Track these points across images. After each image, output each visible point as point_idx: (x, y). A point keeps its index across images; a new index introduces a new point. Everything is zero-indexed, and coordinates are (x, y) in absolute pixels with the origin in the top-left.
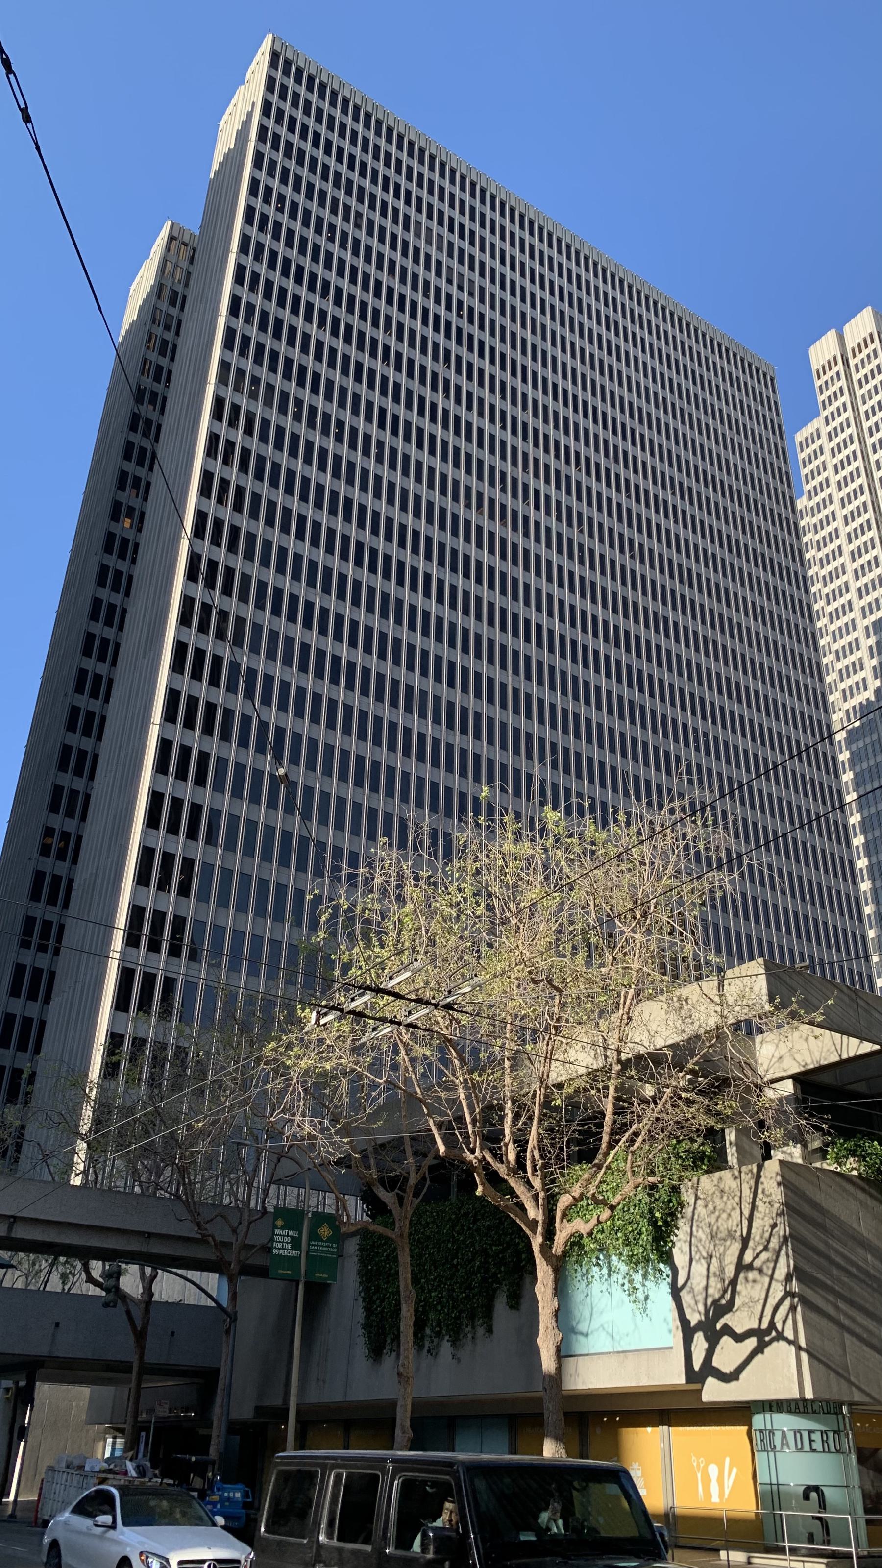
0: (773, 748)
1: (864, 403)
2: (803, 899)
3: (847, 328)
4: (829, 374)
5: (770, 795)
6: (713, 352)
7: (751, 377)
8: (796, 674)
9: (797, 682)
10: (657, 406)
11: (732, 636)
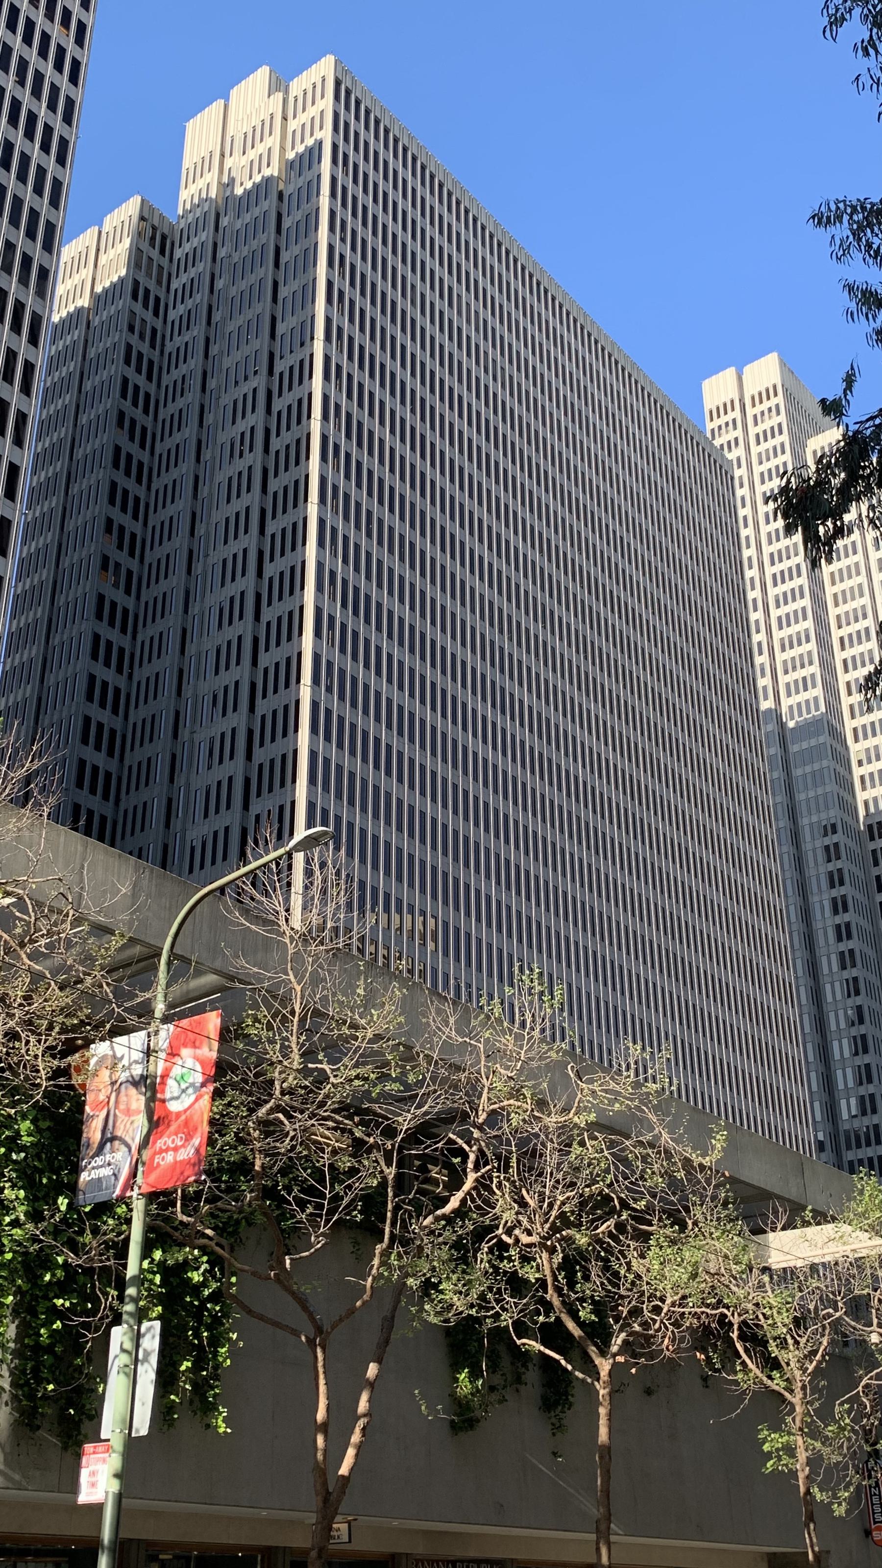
0: (401, 687)
1: (761, 463)
2: (375, 866)
3: (747, 369)
4: (724, 419)
5: (377, 741)
6: (367, 127)
7: (458, 218)
8: (453, 605)
9: (433, 601)
10: (353, 248)
11: (391, 551)
